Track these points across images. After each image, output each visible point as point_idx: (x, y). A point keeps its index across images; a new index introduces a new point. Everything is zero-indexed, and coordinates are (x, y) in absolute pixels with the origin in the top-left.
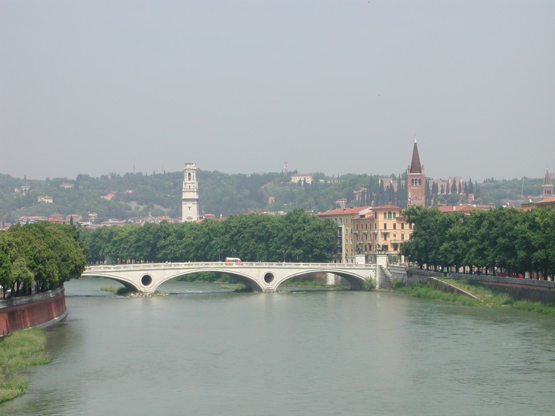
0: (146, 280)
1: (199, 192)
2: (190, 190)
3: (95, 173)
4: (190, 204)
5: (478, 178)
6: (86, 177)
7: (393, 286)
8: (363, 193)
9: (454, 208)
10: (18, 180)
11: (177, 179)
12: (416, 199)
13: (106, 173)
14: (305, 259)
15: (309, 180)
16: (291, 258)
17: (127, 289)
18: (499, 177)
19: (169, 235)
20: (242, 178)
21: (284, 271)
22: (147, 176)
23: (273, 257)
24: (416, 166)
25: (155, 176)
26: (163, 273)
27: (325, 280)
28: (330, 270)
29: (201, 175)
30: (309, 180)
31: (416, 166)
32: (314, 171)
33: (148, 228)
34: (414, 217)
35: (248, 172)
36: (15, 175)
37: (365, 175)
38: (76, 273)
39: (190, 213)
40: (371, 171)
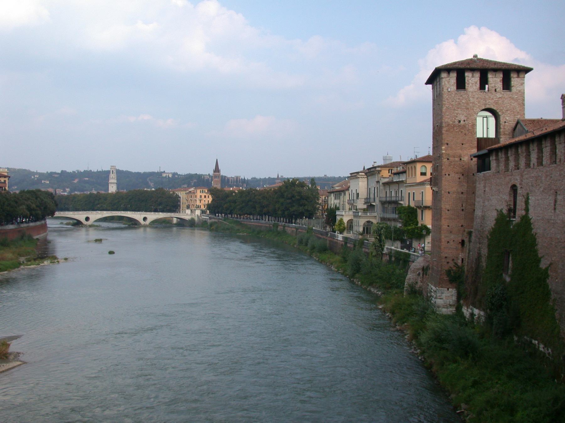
0: (87, 219)
1: (118, 180)
2: (113, 179)
3: (69, 170)
4: (112, 185)
5: (248, 177)
6: (176, 174)
7: (203, 225)
8: (195, 182)
9: (231, 189)
10: (33, 172)
11: (108, 173)
12: (217, 185)
13: (74, 170)
14: (163, 211)
15: (170, 176)
16: (156, 211)
17: (78, 223)
18: (258, 177)
19: (100, 199)
20: (138, 174)
21: (152, 216)
22: (94, 172)
23: (93, 208)
24: (217, 170)
25: (98, 172)
26: (95, 216)
27: (172, 221)
28: (174, 217)
29: (119, 172)
30: (170, 176)
31: (217, 170)
32: (173, 172)
33: (91, 194)
34: (213, 192)
35: (142, 171)
36: (32, 170)
37: (196, 174)
38: (52, 214)
39: (113, 189)
40: (199, 173)
